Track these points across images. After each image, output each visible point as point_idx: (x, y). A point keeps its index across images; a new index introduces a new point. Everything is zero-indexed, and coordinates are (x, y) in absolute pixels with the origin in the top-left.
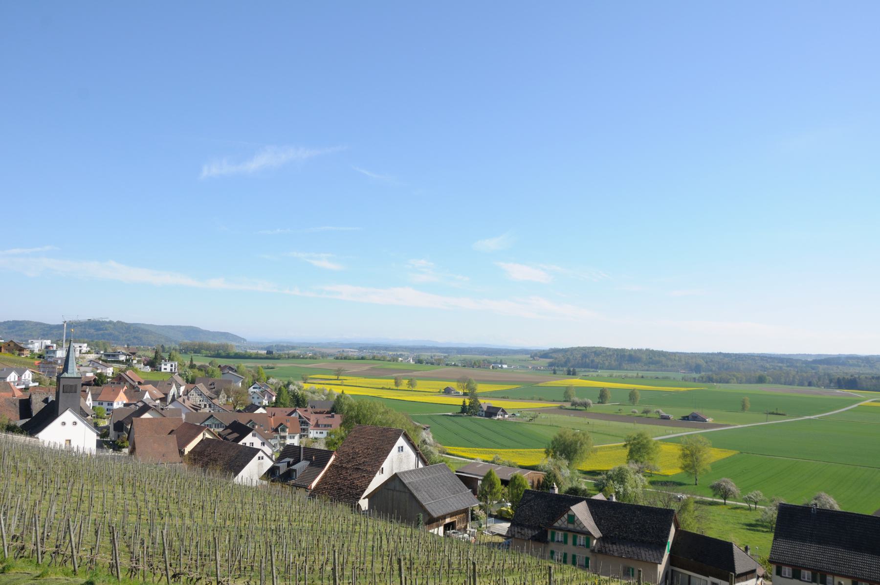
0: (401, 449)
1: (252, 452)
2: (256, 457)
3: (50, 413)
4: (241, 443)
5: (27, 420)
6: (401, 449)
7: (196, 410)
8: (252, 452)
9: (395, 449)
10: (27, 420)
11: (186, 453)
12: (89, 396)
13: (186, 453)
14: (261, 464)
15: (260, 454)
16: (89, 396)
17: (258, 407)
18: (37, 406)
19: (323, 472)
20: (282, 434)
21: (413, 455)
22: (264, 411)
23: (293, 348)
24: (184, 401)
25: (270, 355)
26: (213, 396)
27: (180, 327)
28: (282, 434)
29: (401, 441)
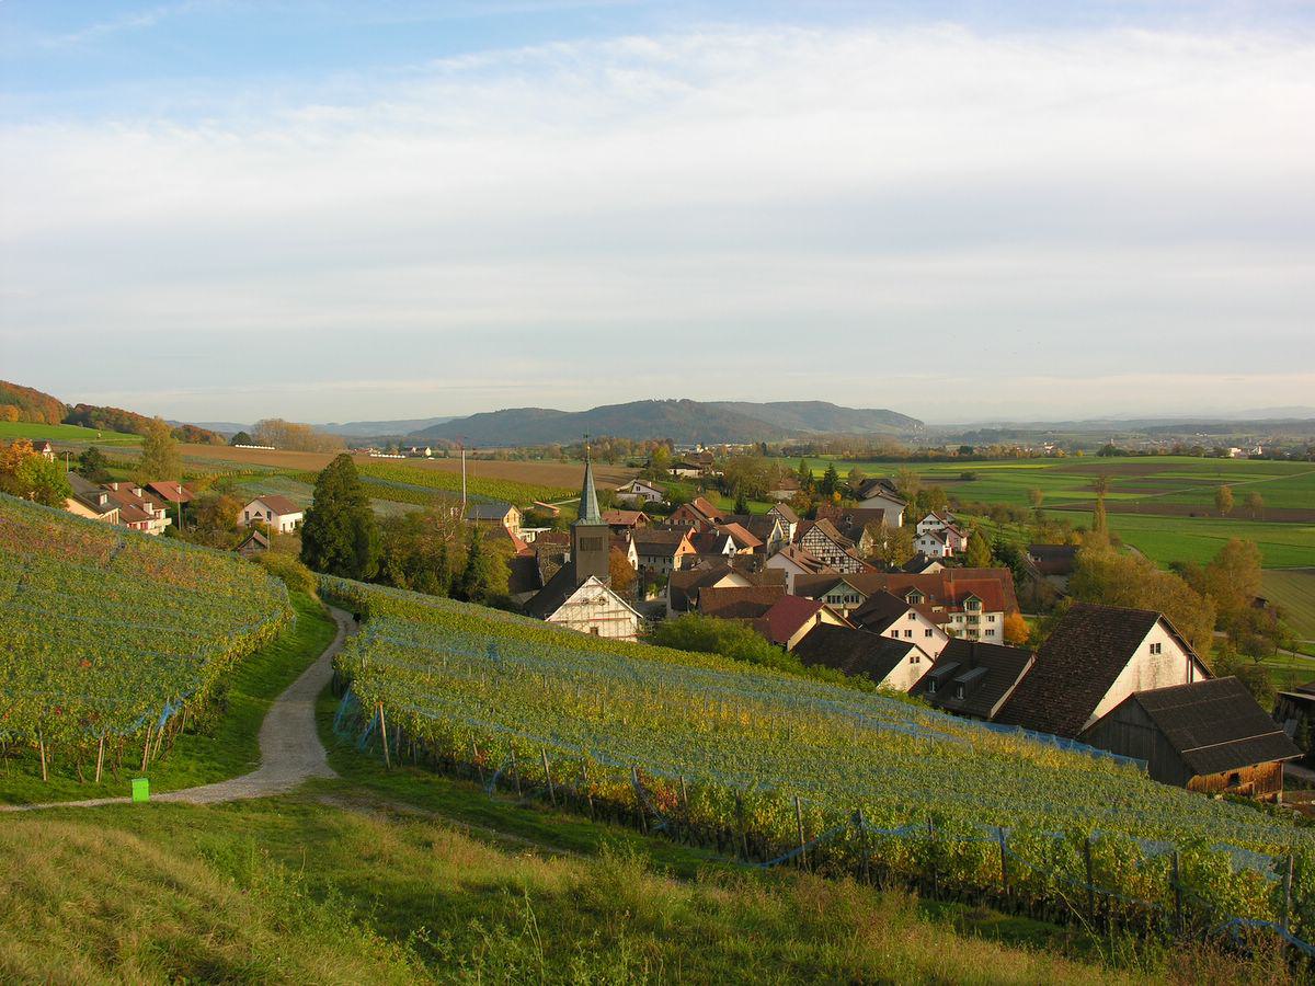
0: (1156, 648)
1: (899, 649)
2: (906, 659)
3: (567, 582)
4: (887, 633)
5: (1103, 708)
6: (1156, 648)
7: (815, 569)
8: (899, 649)
9: (1143, 650)
10: (1103, 708)
11: (790, 647)
12: (632, 548)
13: (790, 647)
14: (917, 669)
15: (914, 652)
16: (632, 548)
17: (931, 561)
18: (547, 570)
19: (1013, 688)
20: (971, 613)
21: (1180, 658)
22: (940, 567)
23: (1013, 434)
24: (792, 552)
25: (965, 454)
26: (846, 540)
27: (796, 404)
28: (971, 613)
29: (1157, 633)
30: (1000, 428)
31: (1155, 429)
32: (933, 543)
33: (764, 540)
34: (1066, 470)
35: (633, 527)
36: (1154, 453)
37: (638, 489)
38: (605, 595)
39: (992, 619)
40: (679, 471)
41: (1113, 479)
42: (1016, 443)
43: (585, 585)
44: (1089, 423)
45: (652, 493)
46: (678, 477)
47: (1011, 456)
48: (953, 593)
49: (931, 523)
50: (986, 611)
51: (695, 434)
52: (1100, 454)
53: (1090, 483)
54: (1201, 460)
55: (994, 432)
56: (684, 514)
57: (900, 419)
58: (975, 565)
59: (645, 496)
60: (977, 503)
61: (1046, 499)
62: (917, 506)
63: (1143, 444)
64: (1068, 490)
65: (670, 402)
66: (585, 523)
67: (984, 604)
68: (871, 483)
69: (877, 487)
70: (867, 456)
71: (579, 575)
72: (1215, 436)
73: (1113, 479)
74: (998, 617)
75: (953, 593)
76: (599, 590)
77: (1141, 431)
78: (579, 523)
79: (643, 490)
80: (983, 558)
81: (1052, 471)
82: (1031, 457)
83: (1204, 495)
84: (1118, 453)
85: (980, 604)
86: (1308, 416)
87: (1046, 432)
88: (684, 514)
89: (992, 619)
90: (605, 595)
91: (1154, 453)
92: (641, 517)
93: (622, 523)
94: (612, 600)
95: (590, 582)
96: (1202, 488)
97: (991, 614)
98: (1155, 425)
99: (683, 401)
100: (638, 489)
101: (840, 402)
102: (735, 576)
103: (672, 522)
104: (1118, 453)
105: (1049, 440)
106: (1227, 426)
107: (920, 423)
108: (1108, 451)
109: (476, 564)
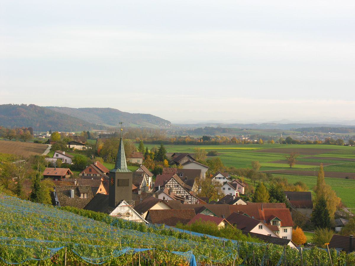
26: (187, 186)
30: (215, 127)
31: (305, 129)
32: (229, 189)
33: (138, 185)
34: (268, 151)
35: (64, 177)
36: (308, 143)
37: (57, 155)
38: (130, 211)
39: (285, 231)
40: (71, 146)
41: (299, 157)
42: (223, 135)
43: (120, 205)
44: (265, 124)
45: (65, 158)
46: (72, 149)
47: (233, 142)
48: (264, 215)
49: (220, 178)
50: (283, 226)
51: (38, 125)
52: (284, 143)
53: (285, 159)
54: (342, 147)
55: (213, 129)
56: (90, 170)
57: (157, 120)
58: (261, 201)
59: (61, 159)
60: (232, 168)
61: (261, 167)
62: (214, 167)
63: (299, 137)
64: (269, 162)
65: (23, 106)
66: (120, 171)
67: (282, 223)
68: (182, 156)
69: (186, 157)
70: (150, 140)
71: (117, 200)
72: (340, 134)
73: (299, 157)
74: (289, 229)
75: (264, 215)
76: (127, 209)
77: (297, 130)
78: (117, 171)
79: (60, 156)
80: (266, 197)
81: (260, 151)
82: (245, 143)
83: (349, 167)
84: (294, 142)
85: (280, 222)
86: (352, 124)
87: (242, 130)
88: (90, 170)
89: (285, 231)
90: (130, 211)
91: (315, 143)
92: (68, 173)
93: (57, 175)
94: (134, 215)
95: (123, 204)
96: (348, 163)
97: (285, 228)
98: (305, 127)
99: (31, 106)
100: (57, 155)
101: (123, 109)
102: (161, 204)
103: (83, 174)
104: (294, 142)
105: (245, 134)
106: (206, 128)
107: (168, 122)
108: (289, 141)
109: (38, 195)
